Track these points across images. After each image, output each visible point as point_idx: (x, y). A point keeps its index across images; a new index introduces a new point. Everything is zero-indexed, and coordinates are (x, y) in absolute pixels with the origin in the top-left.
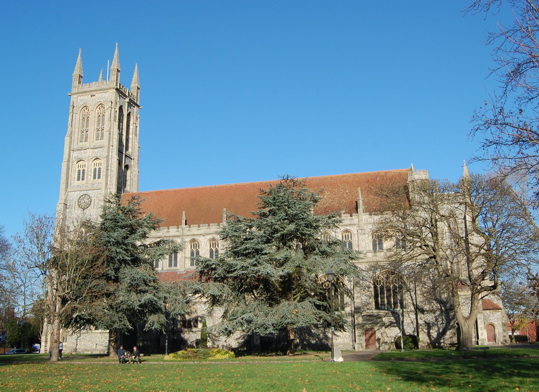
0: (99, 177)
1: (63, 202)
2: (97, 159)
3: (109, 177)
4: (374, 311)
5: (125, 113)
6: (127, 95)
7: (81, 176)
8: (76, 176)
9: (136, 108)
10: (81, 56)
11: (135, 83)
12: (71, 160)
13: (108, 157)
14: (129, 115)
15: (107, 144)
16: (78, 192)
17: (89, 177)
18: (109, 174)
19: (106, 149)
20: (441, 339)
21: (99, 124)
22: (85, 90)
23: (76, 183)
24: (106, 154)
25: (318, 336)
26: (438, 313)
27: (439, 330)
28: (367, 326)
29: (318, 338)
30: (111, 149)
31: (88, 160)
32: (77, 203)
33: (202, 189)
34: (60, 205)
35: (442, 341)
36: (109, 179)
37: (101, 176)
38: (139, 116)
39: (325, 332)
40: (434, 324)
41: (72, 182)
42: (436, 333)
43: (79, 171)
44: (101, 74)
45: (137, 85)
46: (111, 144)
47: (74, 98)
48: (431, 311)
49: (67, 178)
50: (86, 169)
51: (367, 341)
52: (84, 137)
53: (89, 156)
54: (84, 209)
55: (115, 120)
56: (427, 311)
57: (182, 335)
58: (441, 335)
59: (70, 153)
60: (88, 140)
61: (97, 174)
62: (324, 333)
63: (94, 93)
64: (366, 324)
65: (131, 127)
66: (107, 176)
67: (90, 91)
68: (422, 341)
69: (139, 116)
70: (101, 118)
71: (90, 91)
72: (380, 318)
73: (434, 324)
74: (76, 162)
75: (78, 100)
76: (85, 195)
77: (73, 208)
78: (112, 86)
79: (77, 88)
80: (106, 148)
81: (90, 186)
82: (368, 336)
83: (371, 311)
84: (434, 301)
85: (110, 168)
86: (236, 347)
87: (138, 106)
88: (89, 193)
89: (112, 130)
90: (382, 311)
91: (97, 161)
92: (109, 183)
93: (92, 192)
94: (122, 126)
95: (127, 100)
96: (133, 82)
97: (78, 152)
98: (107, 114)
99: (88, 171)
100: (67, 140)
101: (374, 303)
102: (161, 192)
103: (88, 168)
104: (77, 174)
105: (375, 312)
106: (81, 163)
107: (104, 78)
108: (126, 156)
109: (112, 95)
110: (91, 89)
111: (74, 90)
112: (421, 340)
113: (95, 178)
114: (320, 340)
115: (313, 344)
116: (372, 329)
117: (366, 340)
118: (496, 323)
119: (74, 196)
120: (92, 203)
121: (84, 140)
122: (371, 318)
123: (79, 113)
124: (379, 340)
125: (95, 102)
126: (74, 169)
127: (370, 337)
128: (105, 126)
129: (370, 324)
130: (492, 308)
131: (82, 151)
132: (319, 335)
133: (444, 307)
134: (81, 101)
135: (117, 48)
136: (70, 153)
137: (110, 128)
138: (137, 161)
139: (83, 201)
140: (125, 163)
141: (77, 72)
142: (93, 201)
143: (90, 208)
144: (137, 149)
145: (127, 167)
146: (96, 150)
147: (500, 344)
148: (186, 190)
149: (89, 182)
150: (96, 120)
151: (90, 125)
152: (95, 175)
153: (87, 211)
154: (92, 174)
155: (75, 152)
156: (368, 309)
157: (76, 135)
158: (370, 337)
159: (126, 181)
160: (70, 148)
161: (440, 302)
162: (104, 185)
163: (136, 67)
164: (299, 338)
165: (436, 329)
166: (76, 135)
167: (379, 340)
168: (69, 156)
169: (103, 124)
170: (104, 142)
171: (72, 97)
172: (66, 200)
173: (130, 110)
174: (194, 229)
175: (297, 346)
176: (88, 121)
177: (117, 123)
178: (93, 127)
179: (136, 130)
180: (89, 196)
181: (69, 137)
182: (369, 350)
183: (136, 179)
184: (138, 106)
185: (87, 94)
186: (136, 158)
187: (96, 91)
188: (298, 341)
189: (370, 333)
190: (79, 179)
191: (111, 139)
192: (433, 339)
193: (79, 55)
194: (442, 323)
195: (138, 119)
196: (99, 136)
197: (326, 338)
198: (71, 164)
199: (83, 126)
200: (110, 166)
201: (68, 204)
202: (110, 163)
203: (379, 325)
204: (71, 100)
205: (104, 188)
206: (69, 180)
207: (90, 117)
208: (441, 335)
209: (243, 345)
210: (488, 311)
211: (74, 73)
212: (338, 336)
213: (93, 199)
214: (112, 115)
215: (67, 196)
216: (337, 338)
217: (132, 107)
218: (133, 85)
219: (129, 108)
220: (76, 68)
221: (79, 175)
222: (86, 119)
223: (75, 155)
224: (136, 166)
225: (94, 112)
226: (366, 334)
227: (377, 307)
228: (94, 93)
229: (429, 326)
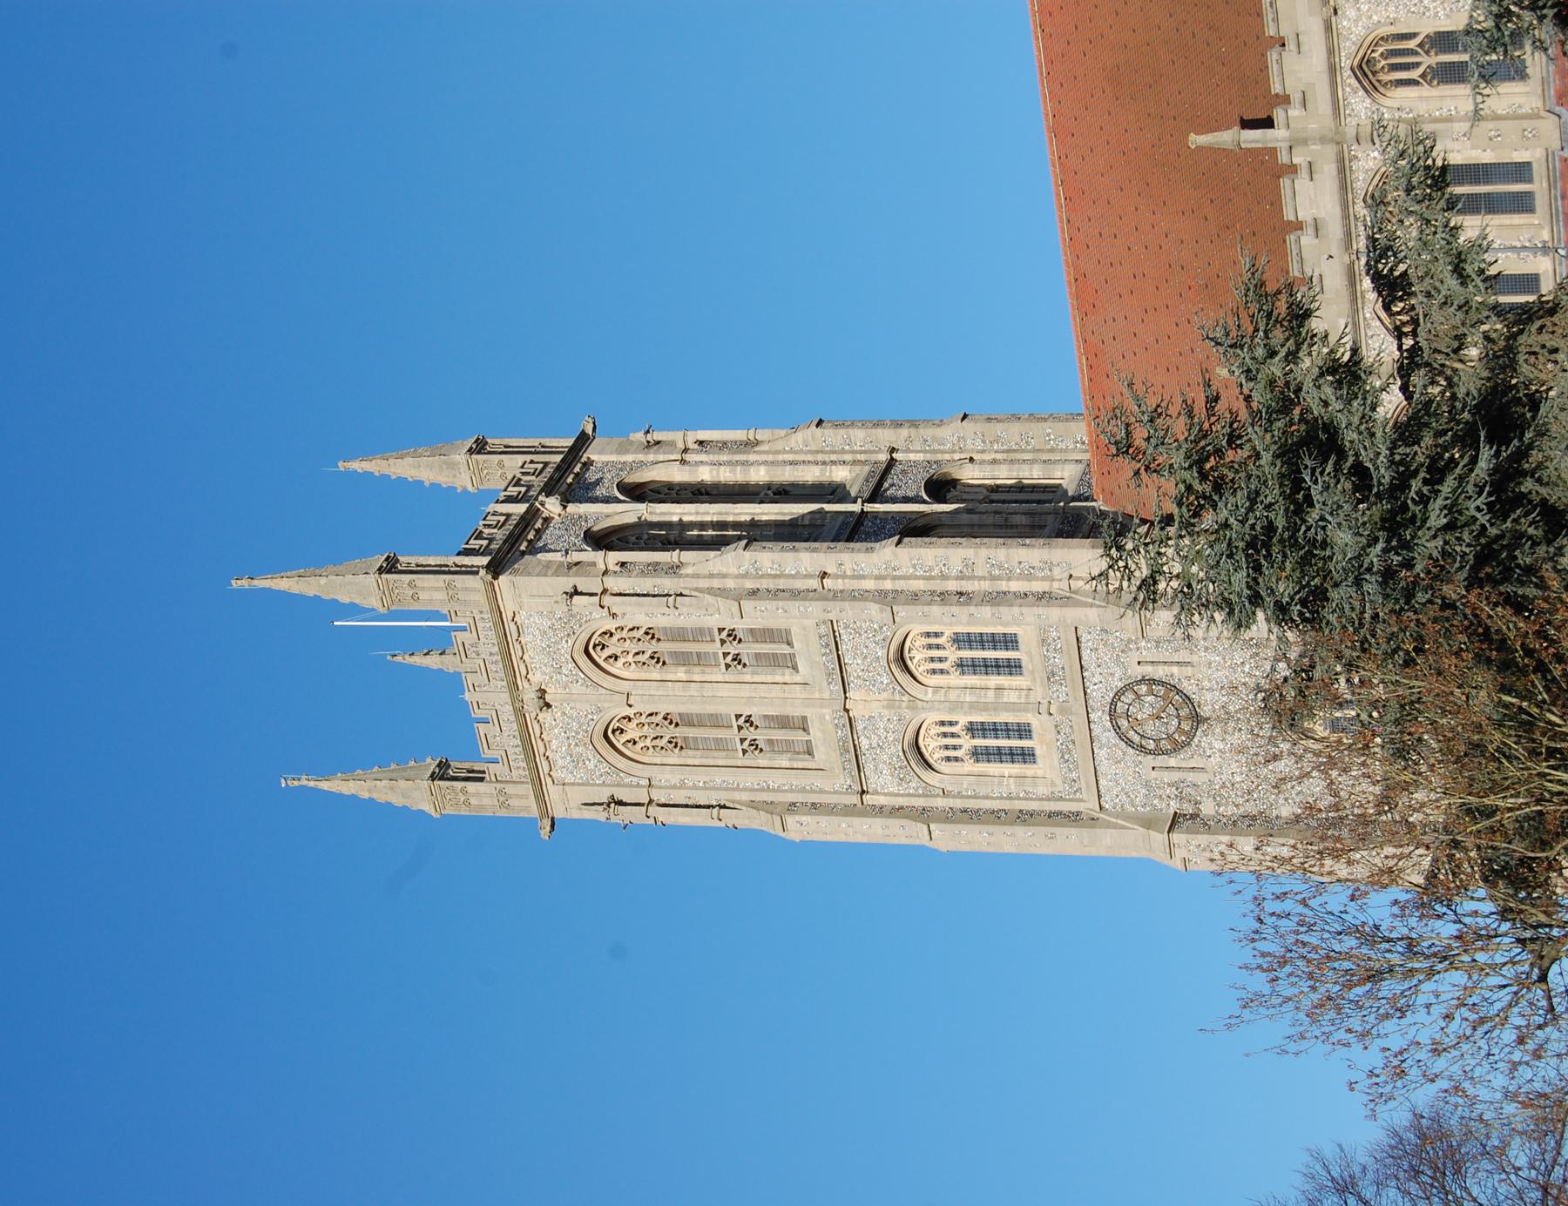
0: (1010, 642)
1: (1159, 838)
2: (901, 660)
3: (1003, 586)
5: (628, 513)
7: (1004, 742)
8: (1008, 769)
9: (593, 454)
10: (326, 775)
11: (452, 466)
12: (920, 802)
14: (637, 492)
15: (815, 609)
16: (1101, 754)
17: (1012, 697)
18: (985, 586)
19: (845, 613)
21: (700, 660)
22: (513, 745)
23: (1045, 777)
24: (873, 609)
31: (913, 708)
32: (1161, 760)
33: (1048, 37)
34: (1180, 853)
36: (1015, 586)
37: (999, 630)
41: (1043, 790)
43: (978, 754)
44: (418, 660)
45: (460, 457)
46: (814, 583)
47: (566, 803)
50: (963, 720)
52: (779, 735)
53: (891, 705)
54: (1197, 719)
55: (674, 569)
59: (880, 811)
60: (796, 711)
61: (991, 655)
63: (529, 695)
65: (705, 475)
66: (997, 599)
67: (520, 713)
70: (658, 649)
71: (520, 713)
74: (928, 776)
76: (1112, 714)
77: (1191, 777)
78: (481, 598)
79: (510, 789)
80: (835, 610)
81: (1066, 692)
85: (952, 586)
87: (583, 440)
88: (1100, 694)
89: (730, 584)
91: (918, 658)
92: (1038, 586)
93: (1094, 676)
94: (702, 526)
95: (552, 506)
96: (443, 479)
97: (869, 768)
98: (639, 614)
99: (974, 707)
100: (800, 828)
102: (1079, 280)
103: (956, 706)
104: (994, 768)
106: (930, 745)
107: (440, 642)
108: (876, 495)
109: (529, 594)
110: (507, 712)
111: (523, 803)
113: (1013, 667)
119: (1125, 776)
120: (1160, 672)
121: (799, 736)
123: (647, 772)
125: (577, 688)
128: (713, 622)
134: (577, 761)
135: (259, 583)
136: (880, 811)
137: (722, 593)
138: (904, 432)
139: (1150, 728)
141: (415, 793)
142: (1148, 670)
143: (1188, 688)
145: (940, 487)
146: (854, 665)
148: (1060, 131)
149: (1039, 694)
150: (681, 674)
151: (710, 709)
152: (997, 667)
153: (1209, 702)
154: (994, 680)
155: (873, 782)
157: (775, 779)
159: (1020, 488)
160: (849, 811)
162: (1054, 613)
163: (357, 466)
166: (775, 779)
168: (896, 812)
169: (699, 634)
170: (802, 621)
171: (559, 814)
172: (1148, 823)
173: (608, 488)
174: (1300, 70)
176: (687, 720)
177: (688, 556)
178: (724, 691)
179: (724, 445)
180: (1119, 694)
181: (790, 820)
183: (1011, 433)
184: (583, 440)
185: (535, 729)
186: (886, 437)
187: (514, 687)
190: (1027, 756)
191: (782, 584)
193: (324, 785)
195: (657, 436)
196: (774, 652)
198: (940, 803)
199: (721, 745)
200: (938, 586)
201: (1174, 805)
202: (919, 585)
204: (576, 814)
205: (1072, 614)
206: (1033, 806)
207: (663, 709)
211: (428, 808)
214: (646, 584)
217: (591, 476)
218: (463, 480)
219: (600, 491)
220: (397, 801)
221: (999, 755)
222: (677, 731)
223: (886, 783)
224: (929, 432)
228: (529, 695)
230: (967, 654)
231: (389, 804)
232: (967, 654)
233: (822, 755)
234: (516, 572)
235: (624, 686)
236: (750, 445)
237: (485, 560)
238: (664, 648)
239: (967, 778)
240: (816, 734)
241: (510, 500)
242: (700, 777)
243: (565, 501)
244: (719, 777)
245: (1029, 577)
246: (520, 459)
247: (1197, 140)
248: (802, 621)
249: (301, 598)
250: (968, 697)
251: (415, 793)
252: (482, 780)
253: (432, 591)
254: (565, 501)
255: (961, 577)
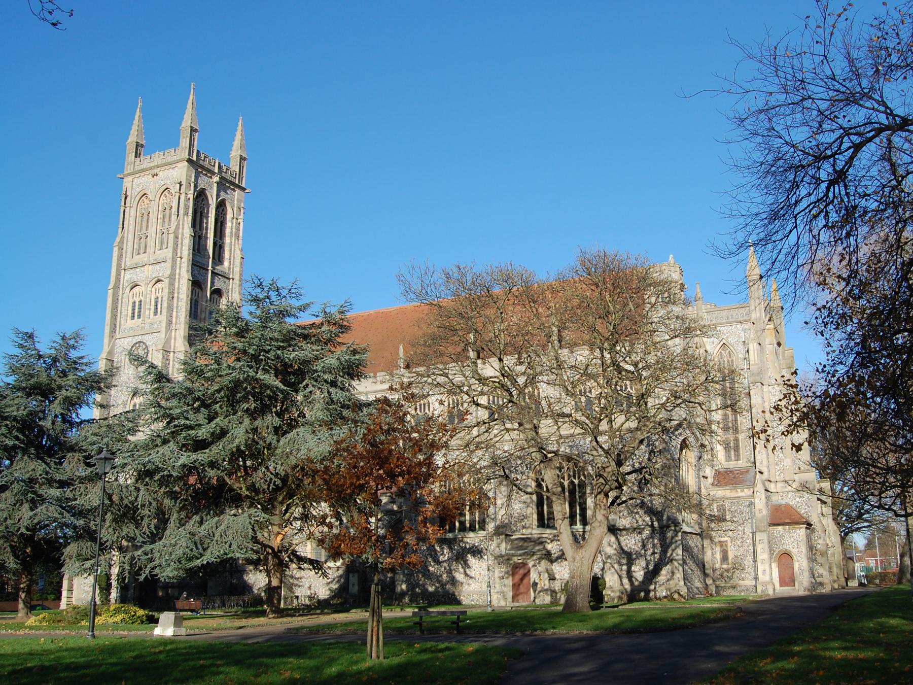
2: (159, 281)
4: (534, 532)
5: (213, 203)
6: (216, 171)
9: (237, 191)
10: (141, 110)
13: (172, 277)
14: (221, 206)
15: (170, 255)
16: (130, 339)
17: (147, 312)
19: (168, 265)
20: (651, 584)
23: (130, 323)
25: (438, 578)
26: (647, 532)
27: (647, 565)
28: (515, 559)
29: (439, 582)
30: (178, 263)
35: (652, 587)
38: (242, 205)
39: (451, 570)
40: (639, 555)
41: (123, 322)
42: (642, 573)
45: (239, 153)
46: (179, 255)
47: (127, 183)
48: (635, 529)
49: (114, 317)
51: (516, 587)
55: (186, 214)
56: (625, 529)
57: (246, 578)
58: (652, 574)
60: (148, 250)
62: (450, 572)
63: (155, 171)
64: (513, 555)
67: (151, 168)
68: (611, 587)
69: (242, 205)
72: (542, 543)
73: (639, 555)
74: (128, 289)
75: (133, 185)
76: (140, 342)
80: (169, 261)
82: (518, 577)
83: (529, 531)
84: (641, 512)
85: (176, 295)
86: (326, 597)
87: (243, 189)
89: (180, 231)
90: (548, 531)
94: (207, 223)
95: (216, 179)
96: (234, 148)
97: (131, 271)
101: (535, 516)
103: (146, 297)
104: (130, 308)
105: (536, 532)
108: (212, 272)
109: (181, 172)
110: (152, 164)
111: (129, 169)
112: (607, 586)
114: (443, 586)
115: (431, 593)
116: (524, 565)
117: (514, 585)
118: (794, 551)
121: (142, 251)
122: (525, 544)
123: (135, 206)
124: (535, 584)
126: (125, 300)
127: (522, 580)
129: (520, 555)
130: (787, 521)
131: (138, 270)
132: (441, 576)
133: (658, 520)
134: (138, 185)
138: (238, 282)
140: (212, 283)
142: (150, 352)
144: (238, 261)
146: (158, 267)
147: (801, 593)
149: (147, 321)
154: (153, 308)
156: (524, 527)
158: (522, 580)
161: (651, 511)
162: (164, 325)
164: (406, 582)
165: (643, 563)
166: (130, 244)
167: (535, 584)
168: (118, 279)
171: (125, 180)
175: (403, 594)
177: (190, 218)
178: (154, 229)
182: (901, 587)
184: (243, 189)
186: (237, 277)
187: (158, 167)
188: (404, 587)
189: (522, 571)
190: (133, 317)
192: (636, 583)
194: (654, 553)
195: (242, 210)
197: (453, 581)
200: (176, 291)
201: (116, 360)
203: (535, 557)
205: (163, 330)
208: (652, 574)
209: (336, 594)
210: (780, 528)
211: (129, 140)
212: (471, 578)
213: (150, 349)
215: (114, 345)
216: (471, 581)
219: (222, 193)
220: (132, 132)
225: (156, 203)
226: (513, 575)
227: (542, 523)
228: (155, 171)
229: (629, 558)
230: (137, 304)
231: (131, 129)
232: (137, 304)
233: (136, 257)
234: (188, 168)
235: (157, 200)
236: (238, 237)
237: (194, 158)
238: (167, 211)
239: (128, 299)
240: (142, 256)
241: (220, 167)
242: (132, 221)
243: (218, 183)
244: (132, 228)
245: (177, 318)
246: (238, 170)
247: (401, 347)
248: (168, 253)
249: (187, 103)
250: (148, 300)
251: (132, 139)
252: (136, 157)
253: (185, 142)
254: (218, 183)
255: (178, 298)
